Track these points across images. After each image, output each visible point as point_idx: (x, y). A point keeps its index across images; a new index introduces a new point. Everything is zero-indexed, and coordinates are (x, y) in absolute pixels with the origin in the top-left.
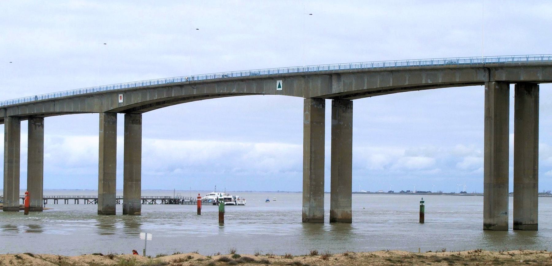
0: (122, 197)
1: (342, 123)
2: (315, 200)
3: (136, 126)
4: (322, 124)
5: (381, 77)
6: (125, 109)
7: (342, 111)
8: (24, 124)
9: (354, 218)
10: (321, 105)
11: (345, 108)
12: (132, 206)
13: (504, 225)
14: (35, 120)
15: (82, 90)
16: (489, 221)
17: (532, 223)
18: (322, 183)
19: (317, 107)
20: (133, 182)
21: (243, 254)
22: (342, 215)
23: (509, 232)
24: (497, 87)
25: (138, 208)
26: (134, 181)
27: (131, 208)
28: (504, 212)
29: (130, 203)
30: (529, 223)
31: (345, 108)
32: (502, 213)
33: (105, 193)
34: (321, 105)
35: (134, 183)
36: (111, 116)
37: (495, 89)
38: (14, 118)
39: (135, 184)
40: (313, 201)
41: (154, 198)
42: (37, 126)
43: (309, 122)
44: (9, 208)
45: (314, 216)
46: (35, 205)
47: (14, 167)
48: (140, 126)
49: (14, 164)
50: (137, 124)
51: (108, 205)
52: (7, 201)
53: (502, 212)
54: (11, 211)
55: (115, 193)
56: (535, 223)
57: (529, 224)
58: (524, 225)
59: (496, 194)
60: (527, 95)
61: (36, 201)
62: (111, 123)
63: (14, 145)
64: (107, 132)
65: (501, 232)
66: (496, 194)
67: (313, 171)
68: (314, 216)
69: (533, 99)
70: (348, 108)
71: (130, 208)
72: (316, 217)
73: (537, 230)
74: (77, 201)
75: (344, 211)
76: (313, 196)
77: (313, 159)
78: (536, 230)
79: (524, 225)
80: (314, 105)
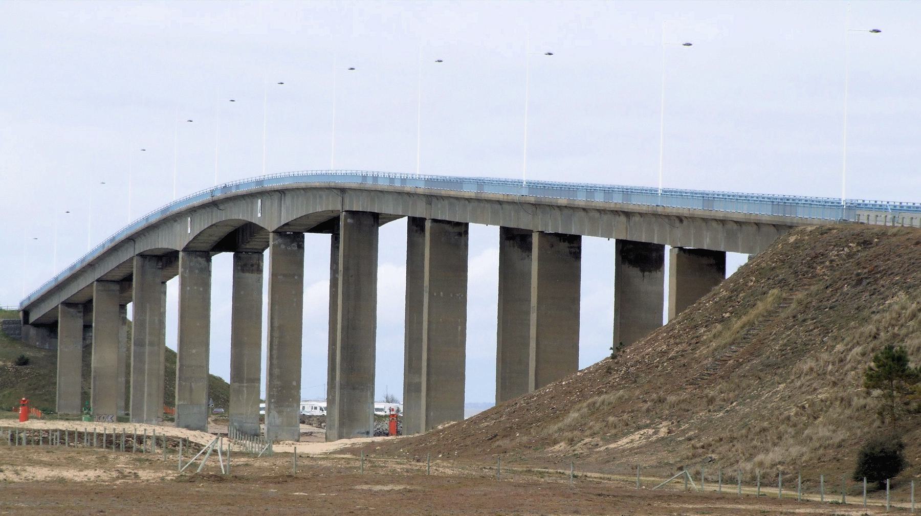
2: (279, 412)
3: (249, 277)
4: (296, 277)
10: (295, 244)
18: (294, 383)
19: (286, 248)
21: (195, 508)
24: (349, 221)
32: (358, 433)
34: (295, 244)
36: (195, 258)
39: (247, 387)
40: (276, 415)
48: (258, 275)
50: (252, 273)
59: (345, 400)
60: (419, 232)
62: (197, 271)
63: (148, 310)
64: (188, 288)
66: (345, 400)
76: (275, 405)
80: (279, 245)
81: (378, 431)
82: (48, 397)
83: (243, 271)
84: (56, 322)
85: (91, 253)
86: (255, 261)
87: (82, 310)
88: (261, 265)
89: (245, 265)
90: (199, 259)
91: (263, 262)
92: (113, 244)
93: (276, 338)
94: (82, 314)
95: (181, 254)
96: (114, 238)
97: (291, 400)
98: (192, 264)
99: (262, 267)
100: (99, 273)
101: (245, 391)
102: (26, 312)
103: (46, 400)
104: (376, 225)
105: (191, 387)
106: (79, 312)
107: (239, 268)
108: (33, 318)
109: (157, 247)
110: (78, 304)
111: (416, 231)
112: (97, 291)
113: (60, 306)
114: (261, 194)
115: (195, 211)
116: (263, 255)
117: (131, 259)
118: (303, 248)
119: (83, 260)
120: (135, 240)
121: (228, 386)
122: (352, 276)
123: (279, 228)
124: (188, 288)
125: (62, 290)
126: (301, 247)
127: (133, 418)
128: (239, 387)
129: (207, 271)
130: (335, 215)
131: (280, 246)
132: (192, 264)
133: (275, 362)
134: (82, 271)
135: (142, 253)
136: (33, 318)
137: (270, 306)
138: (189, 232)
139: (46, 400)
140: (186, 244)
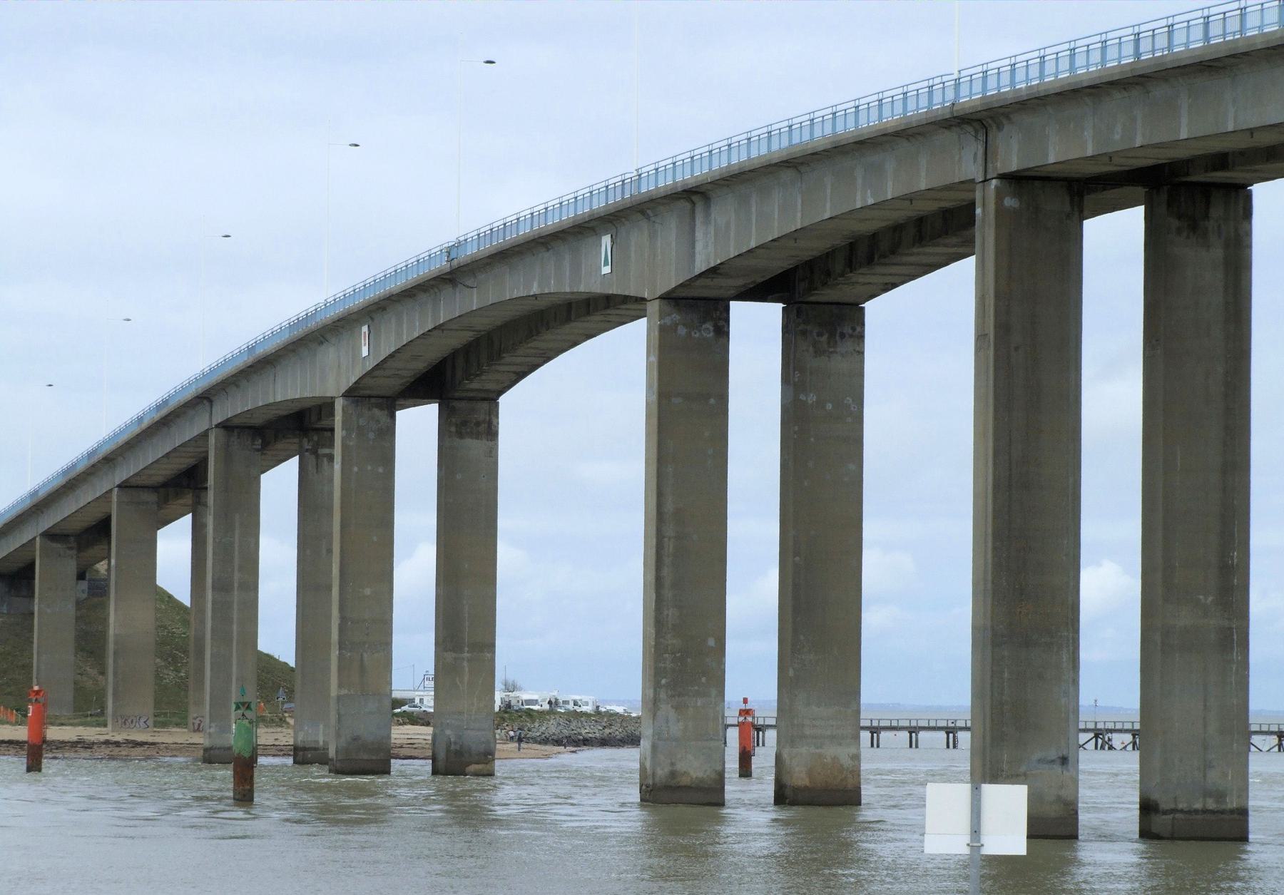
0: (773, 722)
1: (812, 398)
2: (677, 708)
3: (473, 446)
4: (712, 401)
5: (780, 195)
7: (811, 349)
10: (709, 326)
11: (824, 338)
12: (455, 743)
14: (316, 438)
17: (1211, 804)
18: (711, 642)
20: (462, 651)
22: (810, 773)
24: (1009, 202)
25: (482, 750)
26: (466, 649)
27: (453, 747)
28: (1053, 754)
29: (448, 732)
30: (1198, 806)
31: (824, 338)
32: (1039, 761)
33: (346, 691)
34: (709, 326)
35: (466, 655)
36: (369, 409)
37: (1000, 211)
38: (236, 431)
40: (672, 714)
41: (1100, 726)
42: (325, 459)
44: (217, 752)
45: (673, 774)
46: (317, 742)
47: (235, 606)
48: (490, 443)
49: (236, 595)
50: (477, 438)
51: (356, 739)
52: (210, 727)
53: (1038, 755)
54: (219, 763)
56: (1229, 806)
57: (1196, 811)
58: (1165, 813)
60: (1185, 234)
61: (321, 726)
62: (371, 435)
64: (356, 469)
67: (668, 593)
68: (673, 774)
69: (1217, 253)
70: (843, 336)
71: (448, 751)
72: (685, 781)
73: (1244, 838)
74: (951, 735)
75: (820, 756)
76: (670, 693)
77: (670, 546)
79: (1165, 813)
81: (543, 736)
82: (12, 688)
83: (461, 435)
84: (31, 566)
85: (111, 439)
86: (481, 417)
87: (74, 545)
88: (495, 423)
89: (464, 423)
90: (376, 412)
91: (497, 417)
92: (164, 412)
93: (669, 539)
94: (74, 552)
95: (339, 405)
96: (165, 402)
97: (704, 679)
98: (362, 422)
99: (497, 427)
100: (123, 473)
101: (467, 669)
103: (10, 694)
104: (1077, 214)
105: (362, 660)
106: (71, 548)
107: (453, 429)
109: (271, 401)
110: (68, 536)
111: (1179, 231)
112: (119, 503)
113: (38, 539)
114: (611, 222)
115: (384, 309)
116: (497, 405)
117: (204, 435)
118: (727, 334)
119: (91, 454)
120: (213, 398)
121: (292, 669)
122: (1017, 349)
123: (681, 285)
124: (356, 469)
125: (42, 513)
126: (722, 331)
127: (210, 722)
128: (455, 658)
129: (388, 432)
131: (676, 330)
132: (362, 422)
133: (668, 593)
134: (88, 474)
135: (228, 420)
137: (654, 467)
138: (365, 352)
139: (10, 694)
140: (353, 380)
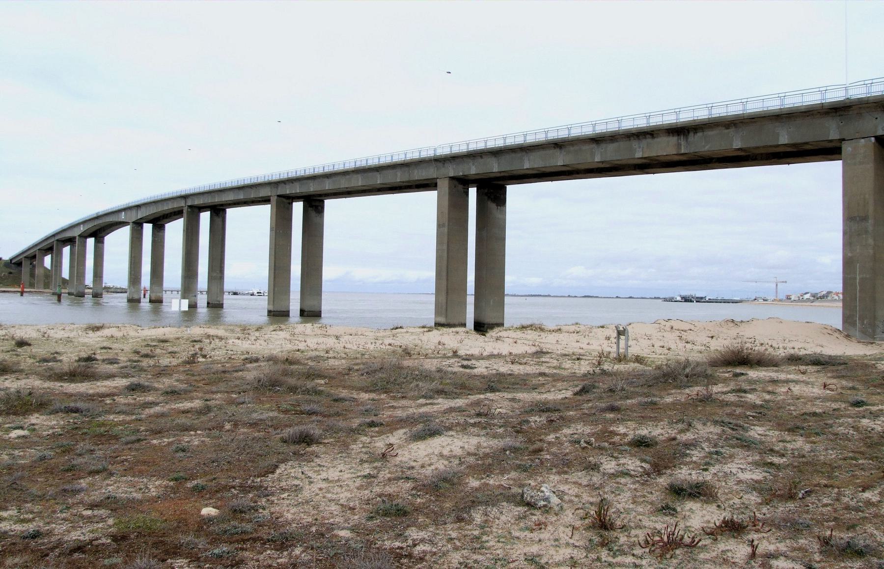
3: (100, 245)
6: (91, 232)
8: (298, 207)
9: (164, 300)
13: (194, 304)
15: (233, 181)
16: (271, 308)
23: (142, 304)
24: (189, 210)
43: (274, 225)
55: (843, 305)
65: (316, 318)
69: (221, 219)
78: (316, 316)
102: (11, 260)
108: (13, 262)
126: (142, 228)
130: (180, 209)
136: (13, 262)
